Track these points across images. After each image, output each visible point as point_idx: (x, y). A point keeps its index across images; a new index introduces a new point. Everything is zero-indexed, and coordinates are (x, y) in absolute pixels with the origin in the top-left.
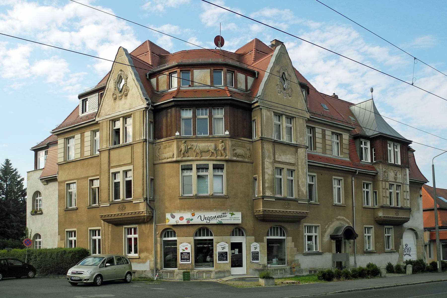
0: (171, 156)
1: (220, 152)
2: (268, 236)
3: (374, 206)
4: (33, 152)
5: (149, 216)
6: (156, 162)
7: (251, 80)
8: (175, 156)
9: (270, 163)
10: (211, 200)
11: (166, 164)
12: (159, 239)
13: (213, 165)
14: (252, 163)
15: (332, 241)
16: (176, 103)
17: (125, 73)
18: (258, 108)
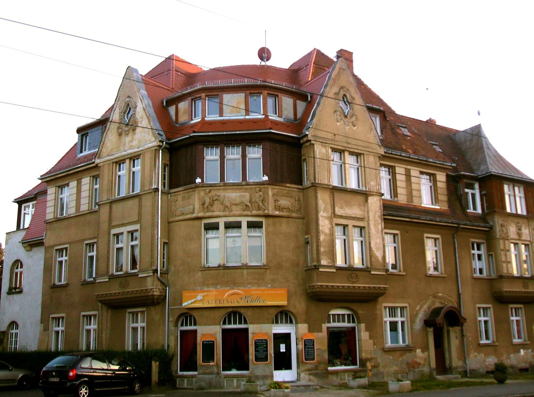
0: (191, 211)
2: (329, 322)
3: (490, 275)
4: (16, 205)
6: (171, 219)
7: (301, 106)
8: (196, 211)
9: (326, 218)
10: (245, 271)
13: (248, 222)
15: (428, 329)
17: (134, 100)
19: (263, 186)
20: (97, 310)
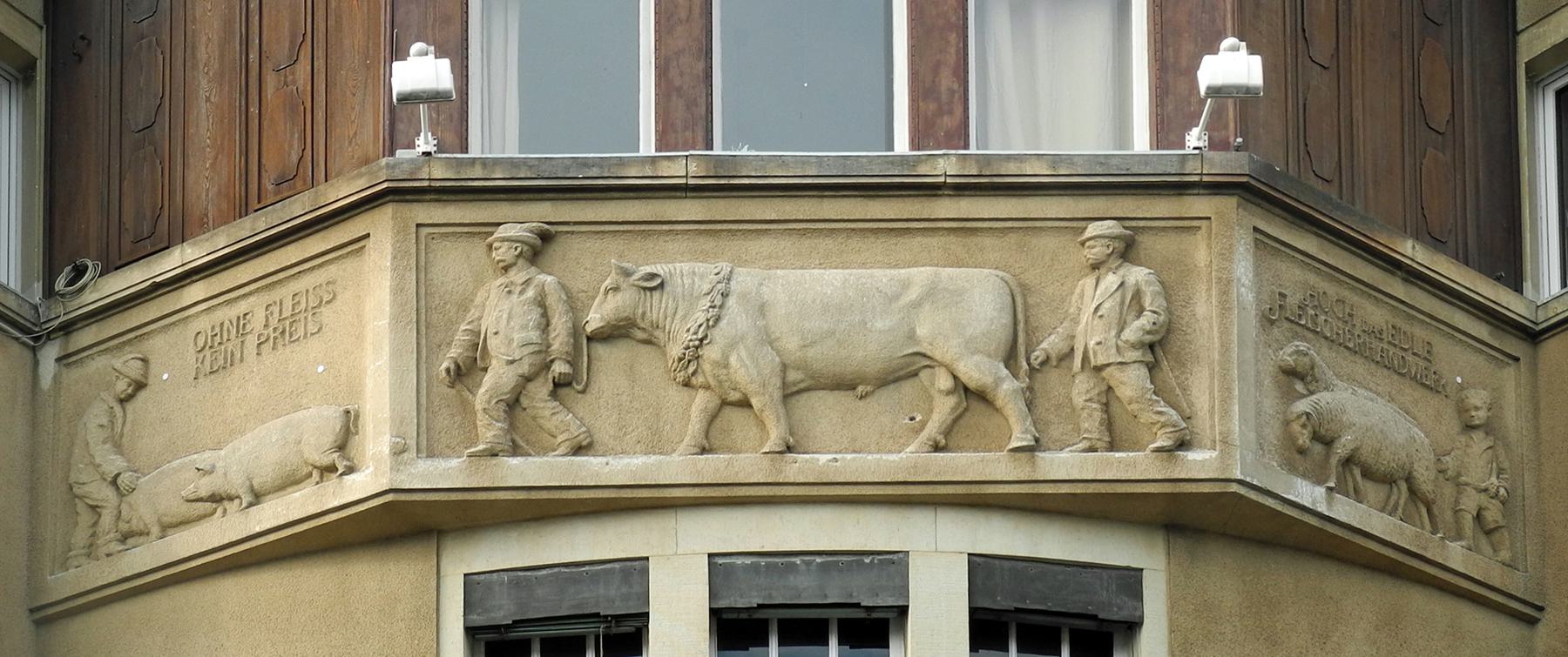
0: (318, 449)
1: (1082, 389)
8: (375, 443)
11: (231, 589)
13: (980, 566)
14: (1527, 616)
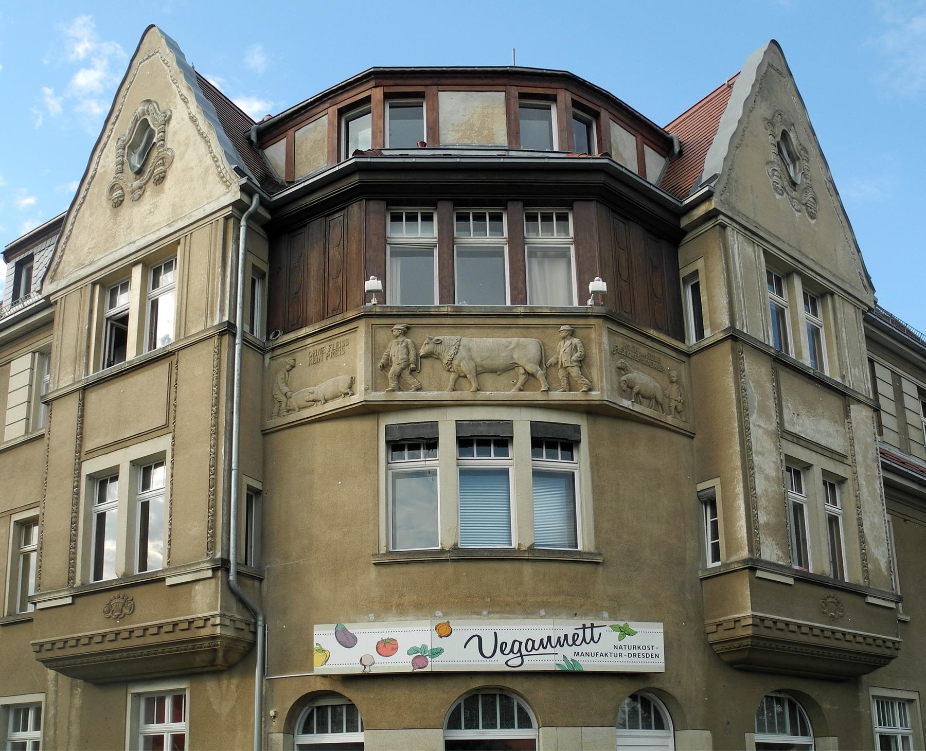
0: (343, 388)
1: (561, 373)
5: (236, 640)
8: (360, 387)
9: (766, 432)
11: (318, 427)
12: (278, 738)
13: (534, 425)
16: (368, 178)
17: (163, 106)
18: (710, 224)
19: (581, 322)
20: (44, 691)
